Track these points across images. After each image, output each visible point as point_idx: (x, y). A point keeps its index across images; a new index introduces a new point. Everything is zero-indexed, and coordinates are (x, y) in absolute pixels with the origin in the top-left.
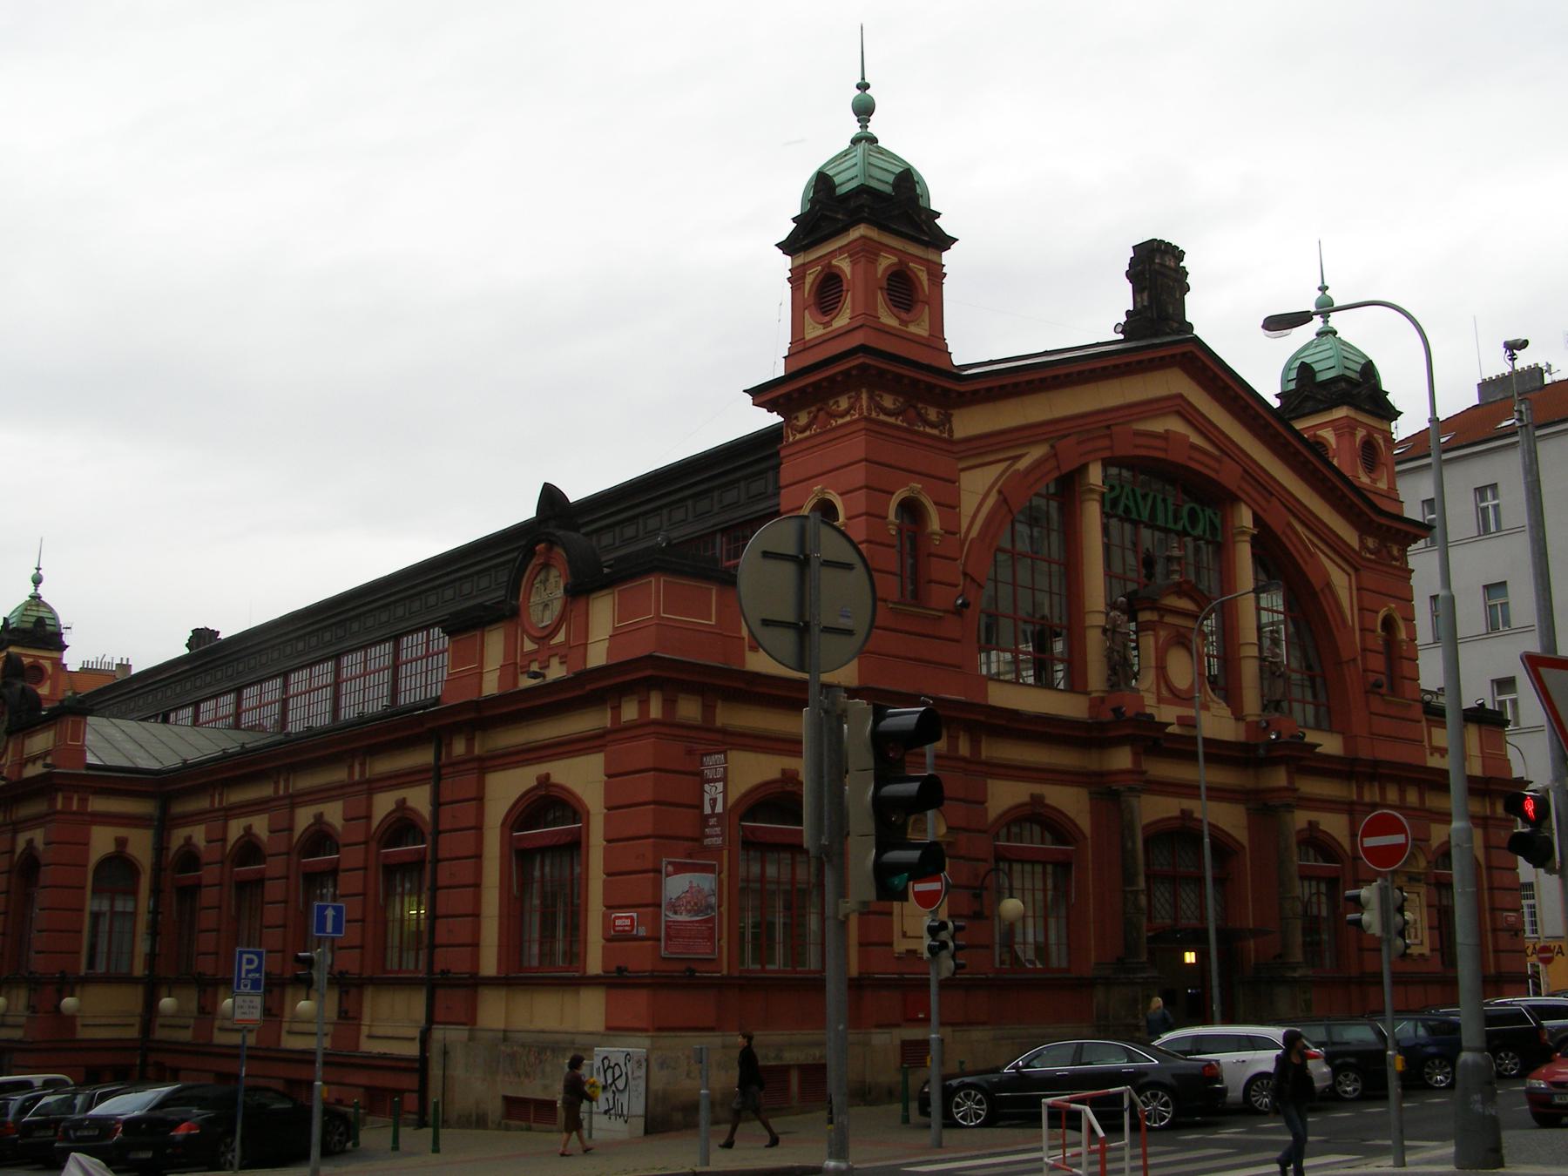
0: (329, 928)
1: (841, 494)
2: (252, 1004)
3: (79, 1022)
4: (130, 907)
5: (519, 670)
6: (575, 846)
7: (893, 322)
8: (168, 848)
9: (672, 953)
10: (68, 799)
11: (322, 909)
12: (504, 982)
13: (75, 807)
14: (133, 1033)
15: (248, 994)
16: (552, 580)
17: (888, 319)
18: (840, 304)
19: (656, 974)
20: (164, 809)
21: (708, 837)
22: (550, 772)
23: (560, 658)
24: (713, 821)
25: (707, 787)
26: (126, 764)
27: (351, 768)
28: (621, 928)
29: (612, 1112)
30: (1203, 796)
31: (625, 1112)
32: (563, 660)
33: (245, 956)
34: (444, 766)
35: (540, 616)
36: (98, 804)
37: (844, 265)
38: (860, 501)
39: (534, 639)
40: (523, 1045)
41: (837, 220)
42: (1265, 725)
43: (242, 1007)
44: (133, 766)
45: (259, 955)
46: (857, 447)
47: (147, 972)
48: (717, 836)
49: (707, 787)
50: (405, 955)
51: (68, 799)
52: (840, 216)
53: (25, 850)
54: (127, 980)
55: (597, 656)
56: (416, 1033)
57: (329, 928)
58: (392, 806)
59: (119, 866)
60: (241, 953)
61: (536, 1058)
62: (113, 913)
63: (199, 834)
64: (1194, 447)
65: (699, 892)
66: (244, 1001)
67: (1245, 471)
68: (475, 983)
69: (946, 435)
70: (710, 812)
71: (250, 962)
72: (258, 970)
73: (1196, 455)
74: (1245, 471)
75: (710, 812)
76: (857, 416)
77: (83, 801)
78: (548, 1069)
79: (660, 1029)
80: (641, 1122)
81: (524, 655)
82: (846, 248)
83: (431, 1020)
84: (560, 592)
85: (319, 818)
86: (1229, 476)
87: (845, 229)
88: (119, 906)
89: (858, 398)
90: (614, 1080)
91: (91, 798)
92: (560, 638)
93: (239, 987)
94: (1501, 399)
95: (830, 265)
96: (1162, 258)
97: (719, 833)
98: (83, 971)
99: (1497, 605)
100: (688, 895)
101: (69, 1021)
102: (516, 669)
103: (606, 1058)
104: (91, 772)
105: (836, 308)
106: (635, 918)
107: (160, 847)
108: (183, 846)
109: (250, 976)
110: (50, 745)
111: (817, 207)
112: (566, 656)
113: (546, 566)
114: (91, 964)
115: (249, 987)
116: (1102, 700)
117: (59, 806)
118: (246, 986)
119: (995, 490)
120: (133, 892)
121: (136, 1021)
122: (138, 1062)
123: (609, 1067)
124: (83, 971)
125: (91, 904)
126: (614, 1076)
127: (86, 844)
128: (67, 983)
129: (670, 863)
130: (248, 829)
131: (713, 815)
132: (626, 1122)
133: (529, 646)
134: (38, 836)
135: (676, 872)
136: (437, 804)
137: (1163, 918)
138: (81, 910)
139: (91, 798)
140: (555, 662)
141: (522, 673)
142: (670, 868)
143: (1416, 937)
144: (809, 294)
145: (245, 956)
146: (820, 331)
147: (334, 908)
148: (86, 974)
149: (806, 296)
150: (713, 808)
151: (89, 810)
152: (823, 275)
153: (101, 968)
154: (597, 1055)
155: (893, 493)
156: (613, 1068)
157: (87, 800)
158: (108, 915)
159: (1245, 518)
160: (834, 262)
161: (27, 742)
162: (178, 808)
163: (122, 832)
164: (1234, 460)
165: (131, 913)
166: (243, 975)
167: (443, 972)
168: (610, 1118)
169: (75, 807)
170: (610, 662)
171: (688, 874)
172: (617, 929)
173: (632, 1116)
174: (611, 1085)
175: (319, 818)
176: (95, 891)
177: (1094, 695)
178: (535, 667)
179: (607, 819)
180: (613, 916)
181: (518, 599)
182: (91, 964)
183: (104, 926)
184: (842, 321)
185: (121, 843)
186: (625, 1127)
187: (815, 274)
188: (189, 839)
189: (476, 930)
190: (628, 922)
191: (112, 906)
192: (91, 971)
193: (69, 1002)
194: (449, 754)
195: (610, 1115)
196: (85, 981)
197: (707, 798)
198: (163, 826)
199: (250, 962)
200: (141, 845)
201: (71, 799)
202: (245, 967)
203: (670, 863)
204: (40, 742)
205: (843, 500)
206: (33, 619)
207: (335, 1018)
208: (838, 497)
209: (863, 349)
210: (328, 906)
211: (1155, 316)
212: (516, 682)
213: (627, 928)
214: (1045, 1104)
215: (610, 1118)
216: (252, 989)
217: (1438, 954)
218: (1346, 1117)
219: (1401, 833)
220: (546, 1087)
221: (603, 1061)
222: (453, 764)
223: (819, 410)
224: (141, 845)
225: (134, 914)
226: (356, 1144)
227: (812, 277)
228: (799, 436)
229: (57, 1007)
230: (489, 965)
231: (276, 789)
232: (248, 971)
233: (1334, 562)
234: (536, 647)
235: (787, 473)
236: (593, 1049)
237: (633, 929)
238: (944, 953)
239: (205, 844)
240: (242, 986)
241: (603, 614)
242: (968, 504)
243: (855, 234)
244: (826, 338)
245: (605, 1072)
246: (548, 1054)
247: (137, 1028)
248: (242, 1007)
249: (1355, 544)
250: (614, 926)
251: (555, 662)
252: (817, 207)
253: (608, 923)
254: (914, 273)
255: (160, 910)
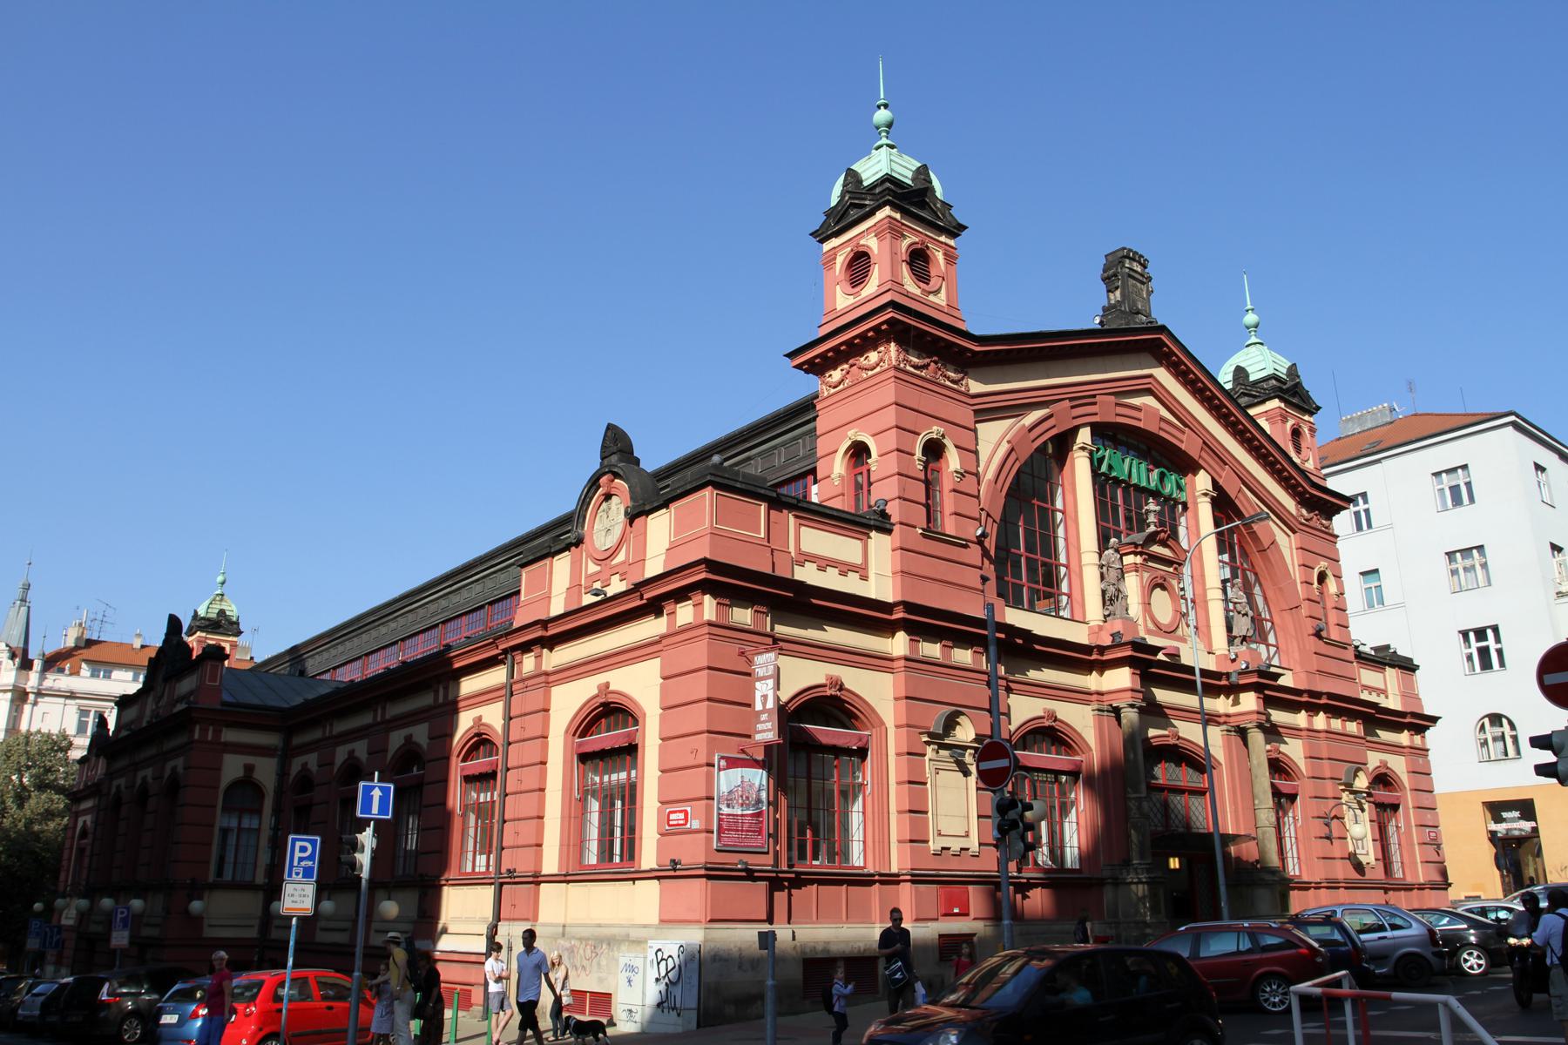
0: (375, 809)
1: (873, 435)
2: (303, 893)
3: (206, 922)
4: (255, 825)
5: (583, 591)
6: (629, 752)
7: (918, 292)
8: (289, 774)
9: (725, 845)
10: (204, 731)
11: (368, 790)
12: (564, 878)
13: (210, 738)
14: (253, 933)
15: (300, 883)
16: (614, 507)
17: (911, 286)
18: (868, 278)
19: (709, 865)
20: (287, 741)
21: (760, 732)
22: (608, 680)
23: (621, 575)
24: (764, 717)
25: (758, 685)
26: (256, 701)
27: (437, 692)
28: (675, 823)
29: (665, 1005)
30: (587, 1013)
31: (678, 1005)
32: (623, 577)
33: (298, 844)
34: (515, 683)
35: (603, 541)
36: (230, 736)
37: (872, 243)
38: (892, 439)
39: (598, 561)
40: (581, 939)
41: (865, 206)
42: (1234, 657)
43: (292, 895)
44: (262, 703)
45: (313, 843)
46: (888, 392)
47: (267, 881)
48: (768, 730)
49: (758, 685)
50: (478, 857)
51: (204, 731)
52: (867, 202)
53: (170, 776)
54: (249, 887)
55: (654, 568)
56: (484, 929)
57: (375, 809)
58: (471, 724)
59: (247, 785)
60: (294, 840)
61: (592, 952)
62: (240, 829)
63: (312, 760)
64: (1162, 419)
65: (750, 786)
66: (295, 889)
67: (1204, 442)
68: (537, 879)
69: (963, 389)
70: (761, 708)
71: (303, 849)
72: (311, 858)
73: (1163, 425)
74: (1204, 442)
75: (761, 708)
76: (887, 366)
77: (217, 733)
78: (604, 962)
79: (712, 921)
80: (694, 1015)
81: (588, 577)
82: (872, 229)
83: (498, 917)
84: (621, 517)
85: (409, 739)
86: (1188, 444)
87: (872, 213)
88: (246, 823)
89: (888, 351)
90: (667, 973)
91: (224, 729)
92: (621, 557)
93: (290, 875)
94: (1359, 433)
95: (858, 245)
96: (1130, 263)
97: (770, 727)
98: (211, 878)
99: (1371, 588)
100: (740, 789)
101: (197, 921)
102: (580, 591)
103: (660, 950)
104: (225, 708)
105: (863, 282)
106: (689, 811)
107: (282, 774)
108: (300, 771)
109: (303, 864)
110: (194, 686)
111: (847, 198)
112: (625, 573)
113: (608, 497)
114: (220, 873)
115: (301, 875)
116: (1100, 628)
117: (196, 736)
118: (297, 874)
119: (1005, 440)
120: (258, 812)
121: (256, 922)
122: (256, 959)
123: (662, 959)
124: (211, 878)
125: (223, 820)
126: (1275, 631)
127: (219, 769)
128: (197, 889)
129: (723, 758)
130: (351, 752)
131: (764, 711)
132: (679, 1015)
133: (593, 568)
134: (179, 762)
135: (729, 767)
136: (508, 718)
137: (1156, 826)
138: (212, 826)
139: (224, 729)
140: (615, 579)
141: (586, 593)
142: (723, 763)
143: (1363, 848)
144: (840, 272)
145: (298, 844)
146: (851, 300)
147: (380, 788)
148: (214, 881)
149: (837, 273)
150: (764, 704)
151: (223, 740)
152: (852, 254)
153: (228, 876)
154: (651, 947)
155: (919, 434)
156: (666, 960)
157: (221, 731)
158: (236, 830)
159: (1202, 481)
160: (862, 242)
161: (177, 685)
162: (297, 740)
163: (250, 760)
164: (1197, 434)
165: (256, 829)
166: (295, 863)
167: (509, 871)
168: (663, 1011)
169: (210, 738)
170: (666, 570)
171: (740, 769)
172: (671, 823)
173: (684, 1009)
174: (664, 977)
175: (409, 739)
176: (225, 809)
177: (1092, 624)
178: (597, 585)
179: (663, 719)
180: (668, 811)
181: (583, 527)
182: (220, 873)
183: (232, 840)
184: (871, 287)
185: (249, 769)
186: (680, 1021)
187: (845, 255)
188: (305, 765)
189: (540, 831)
190: (682, 816)
191: (239, 823)
192: (219, 879)
193: (196, 906)
194: (520, 671)
195: (663, 1008)
196: (214, 887)
197: (758, 695)
198: (286, 754)
199: (303, 849)
200: (266, 772)
201: (207, 730)
202: (298, 854)
203: (723, 758)
204: (186, 685)
205: (876, 442)
206: (217, 611)
207: (416, 917)
208: (870, 438)
209: (892, 304)
210: (374, 787)
211: (1127, 310)
212: (580, 599)
213: (682, 822)
214: (1295, 993)
215: (663, 1011)
216: (303, 877)
217: (1381, 864)
218: (1407, 1010)
219: (1548, 686)
220: (601, 980)
221: (656, 954)
222: (524, 680)
223: (852, 366)
224: (266, 772)
225: (258, 830)
226: (1257, 861)
227: (842, 258)
228: (833, 391)
229: (187, 912)
230: (550, 865)
231: (375, 717)
232: (301, 859)
233: (1277, 525)
234: (598, 568)
235: (821, 425)
236: (646, 942)
237: (686, 824)
238: (1013, 833)
239: (317, 768)
240: (294, 874)
241: (660, 527)
242: (984, 450)
243: (880, 215)
244: (855, 306)
245: (658, 964)
246: (604, 947)
247: (256, 928)
248: (292, 895)
249: (1294, 512)
250: (669, 820)
251: (615, 579)
252: (847, 198)
253: (664, 819)
254: (933, 253)
255: (280, 827)
